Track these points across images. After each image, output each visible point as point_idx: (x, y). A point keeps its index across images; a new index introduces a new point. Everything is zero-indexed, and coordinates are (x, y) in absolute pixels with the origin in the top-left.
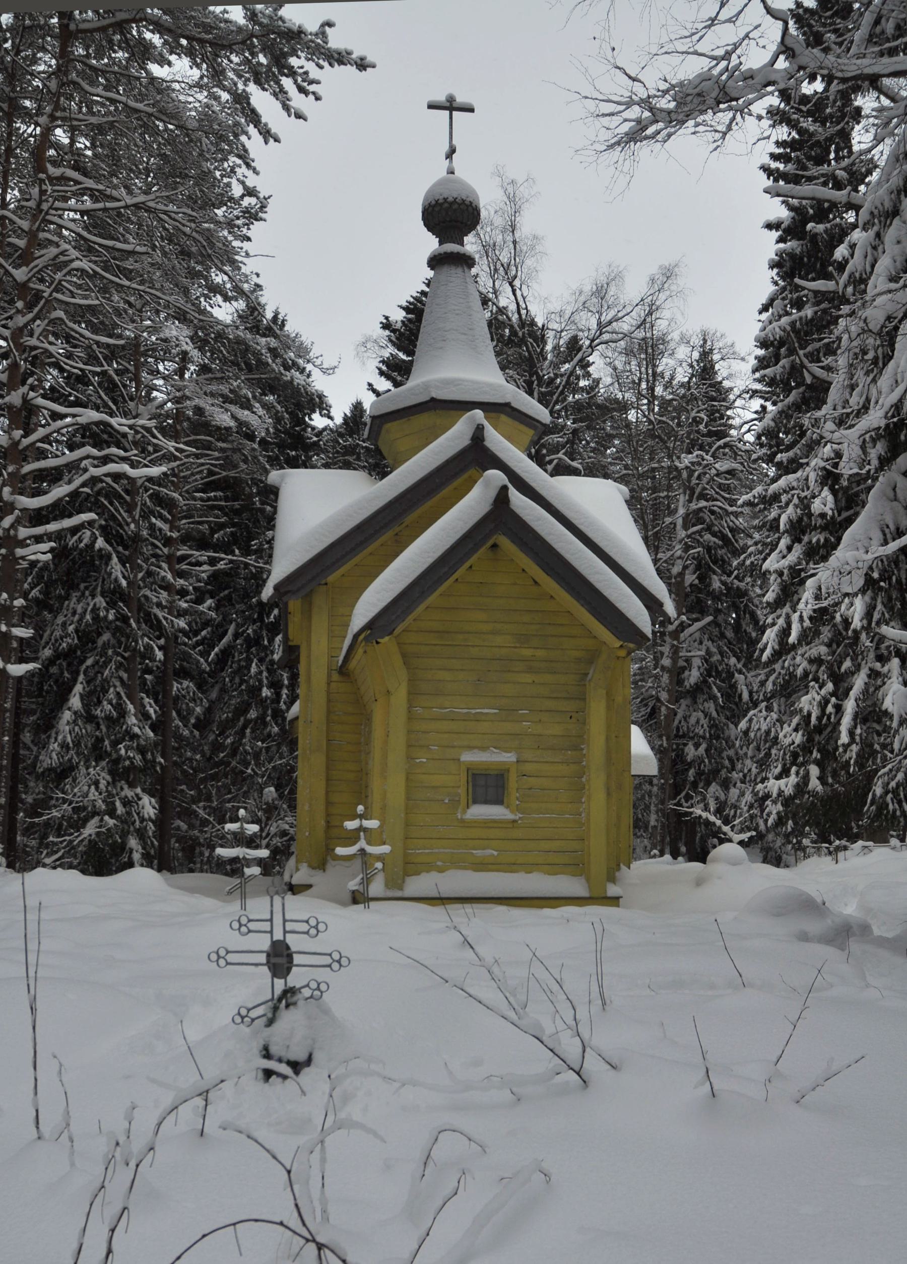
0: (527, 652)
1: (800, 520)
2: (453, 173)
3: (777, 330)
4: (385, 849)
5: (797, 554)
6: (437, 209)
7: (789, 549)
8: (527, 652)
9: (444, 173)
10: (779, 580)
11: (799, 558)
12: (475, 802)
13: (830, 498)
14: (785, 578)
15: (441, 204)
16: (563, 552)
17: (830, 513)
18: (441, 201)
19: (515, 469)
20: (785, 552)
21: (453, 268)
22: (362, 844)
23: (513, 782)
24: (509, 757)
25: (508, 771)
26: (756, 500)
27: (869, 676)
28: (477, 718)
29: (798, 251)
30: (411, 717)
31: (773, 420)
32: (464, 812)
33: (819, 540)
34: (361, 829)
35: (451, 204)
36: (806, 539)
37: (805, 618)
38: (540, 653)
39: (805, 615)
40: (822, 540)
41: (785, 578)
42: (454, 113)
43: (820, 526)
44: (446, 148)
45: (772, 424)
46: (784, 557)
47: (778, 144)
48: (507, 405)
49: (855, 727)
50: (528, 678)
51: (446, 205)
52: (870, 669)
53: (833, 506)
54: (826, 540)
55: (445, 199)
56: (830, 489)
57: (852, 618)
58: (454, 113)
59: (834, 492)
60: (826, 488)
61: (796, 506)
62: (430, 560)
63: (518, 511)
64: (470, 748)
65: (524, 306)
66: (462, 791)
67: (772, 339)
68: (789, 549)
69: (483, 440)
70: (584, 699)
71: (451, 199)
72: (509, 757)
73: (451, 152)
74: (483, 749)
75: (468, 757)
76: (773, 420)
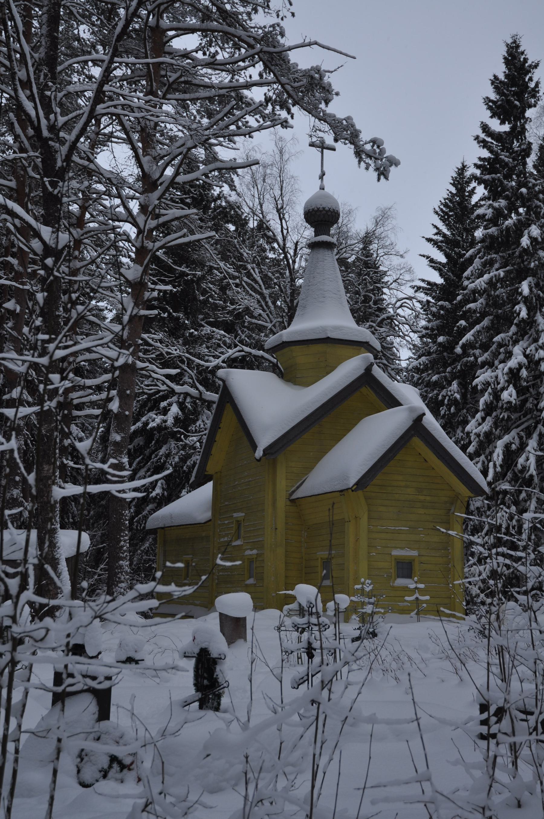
0: (422, 498)
1: (492, 402)
2: (323, 189)
3: (483, 283)
4: (427, 598)
5: (490, 424)
6: (318, 213)
7: (484, 419)
8: (422, 498)
9: (318, 189)
10: (477, 439)
11: (491, 426)
12: (398, 577)
13: (514, 393)
14: (481, 438)
15: (321, 211)
16: (446, 447)
17: (514, 402)
18: (321, 209)
19: (388, 388)
20: (480, 420)
21: (326, 250)
22: (417, 595)
23: (416, 567)
24: (415, 553)
25: (414, 560)
26: (422, 367)
27: (537, 502)
28: (399, 532)
29: (496, 234)
30: (370, 531)
31: (473, 335)
32: (394, 582)
33: (504, 416)
34: (416, 588)
35: (327, 211)
36: (494, 414)
37: (498, 466)
38: (428, 498)
39: (498, 464)
40: (506, 417)
41: (481, 438)
42: (325, 151)
43: (506, 408)
44: (319, 172)
45: (472, 338)
46: (480, 424)
47: (480, 159)
48: (367, 343)
49: (531, 535)
50: (422, 511)
51: (324, 212)
52: (537, 498)
53: (516, 397)
54: (508, 416)
55: (324, 208)
56: (514, 386)
57: (529, 467)
58: (325, 151)
59: (515, 387)
60: (511, 385)
61: (490, 394)
62: (385, 450)
63: (425, 425)
64: (396, 548)
65: (286, 227)
66: (392, 571)
67: (479, 289)
68: (484, 419)
69: (371, 370)
70: (449, 523)
71: (327, 209)
72: (415, 553)
73: (323, 174)
74: (402, 548)
75: (396, 553)
76: (473, 335)
